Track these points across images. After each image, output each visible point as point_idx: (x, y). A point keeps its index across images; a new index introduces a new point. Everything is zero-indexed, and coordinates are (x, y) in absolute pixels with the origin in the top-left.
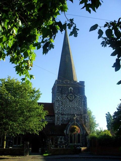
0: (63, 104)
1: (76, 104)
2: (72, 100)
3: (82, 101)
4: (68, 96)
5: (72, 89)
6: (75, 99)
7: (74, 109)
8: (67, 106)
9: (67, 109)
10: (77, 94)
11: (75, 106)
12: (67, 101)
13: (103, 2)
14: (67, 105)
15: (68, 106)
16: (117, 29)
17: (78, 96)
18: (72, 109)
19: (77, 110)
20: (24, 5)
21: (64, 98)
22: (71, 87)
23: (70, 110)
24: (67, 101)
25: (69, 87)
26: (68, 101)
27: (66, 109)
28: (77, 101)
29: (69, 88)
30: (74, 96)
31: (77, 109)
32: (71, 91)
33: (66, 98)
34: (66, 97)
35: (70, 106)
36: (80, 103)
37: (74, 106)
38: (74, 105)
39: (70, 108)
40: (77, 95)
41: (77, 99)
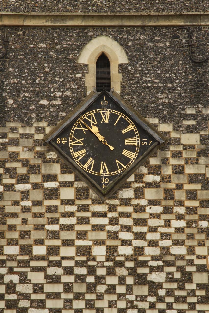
0: (12, 228)
1: (168, 223)
2: (120, 183)
4: (65, 132)
5: (118, 56)
6: (153, 161)
7: (141, 280)
8: (53, 250)
9: (56, 279)
10: (171, 106)
11: (153, 244)
12: (53, 194)
14: (54, 235)
15: (70, 251)
17: (191, 130)
18: (112, 280)
19: (170, 293)
20: (11, 105)
21: (25, 163)
22: (101, 30)
23: (91, 288)
24: (53, 194)
25: (84, 36)
26: (68, 193)
27: (38, 288)
28: (169, 195)
29: (80, 48)
30: (143, 133)
31: (170, 279)
32: (103, 84)
33: (41, 155)
34: (49, 144)
35: (85, 251)
37: (139, 251)
38: (140, 236)
39: (92, 271)
40: (172, 115)
41: (179, 170)
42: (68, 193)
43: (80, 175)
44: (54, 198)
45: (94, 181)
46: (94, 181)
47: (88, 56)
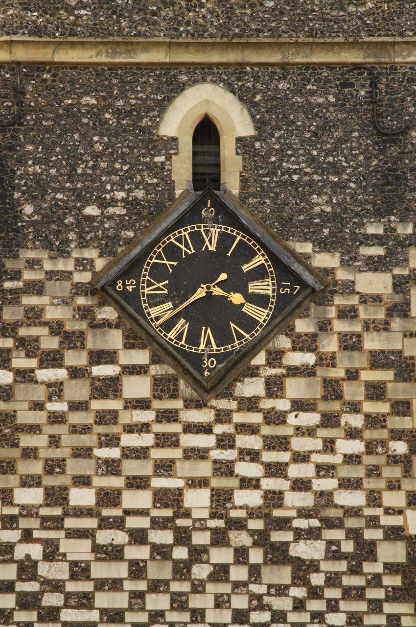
2: (237, 366)
5: (236, 121)
12: (109, 388)
24: (109, 388)
42: (138, 387)
43: (162, 352)
45: (188, 363)
46: (188, 363)
47: (177, 121)
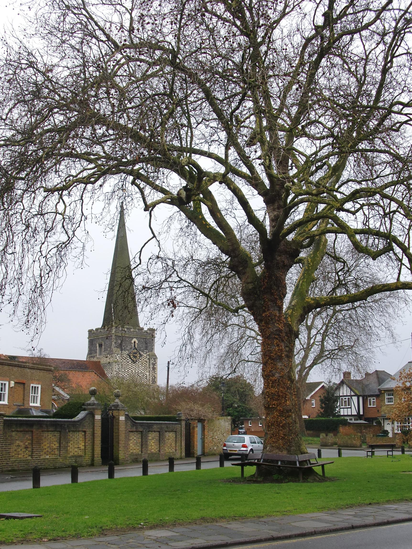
2: (136, 361)
3: (151, 363)
5: (137, 342)
12: (128, 362)
13: (333, 463)
16: (149, 75)
24: (128, 362)
36: (148, 366)
42: (130, 362)
43: (132, 360)
44: (301, 480)
45: (133, 361)
46: (133, 361)
47: (133, 342)
